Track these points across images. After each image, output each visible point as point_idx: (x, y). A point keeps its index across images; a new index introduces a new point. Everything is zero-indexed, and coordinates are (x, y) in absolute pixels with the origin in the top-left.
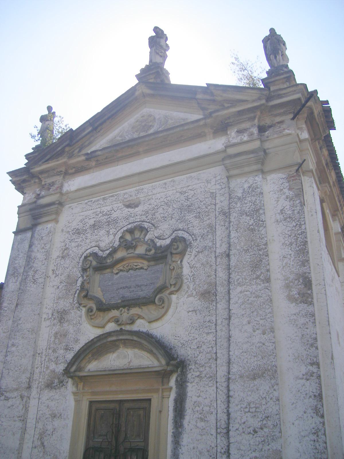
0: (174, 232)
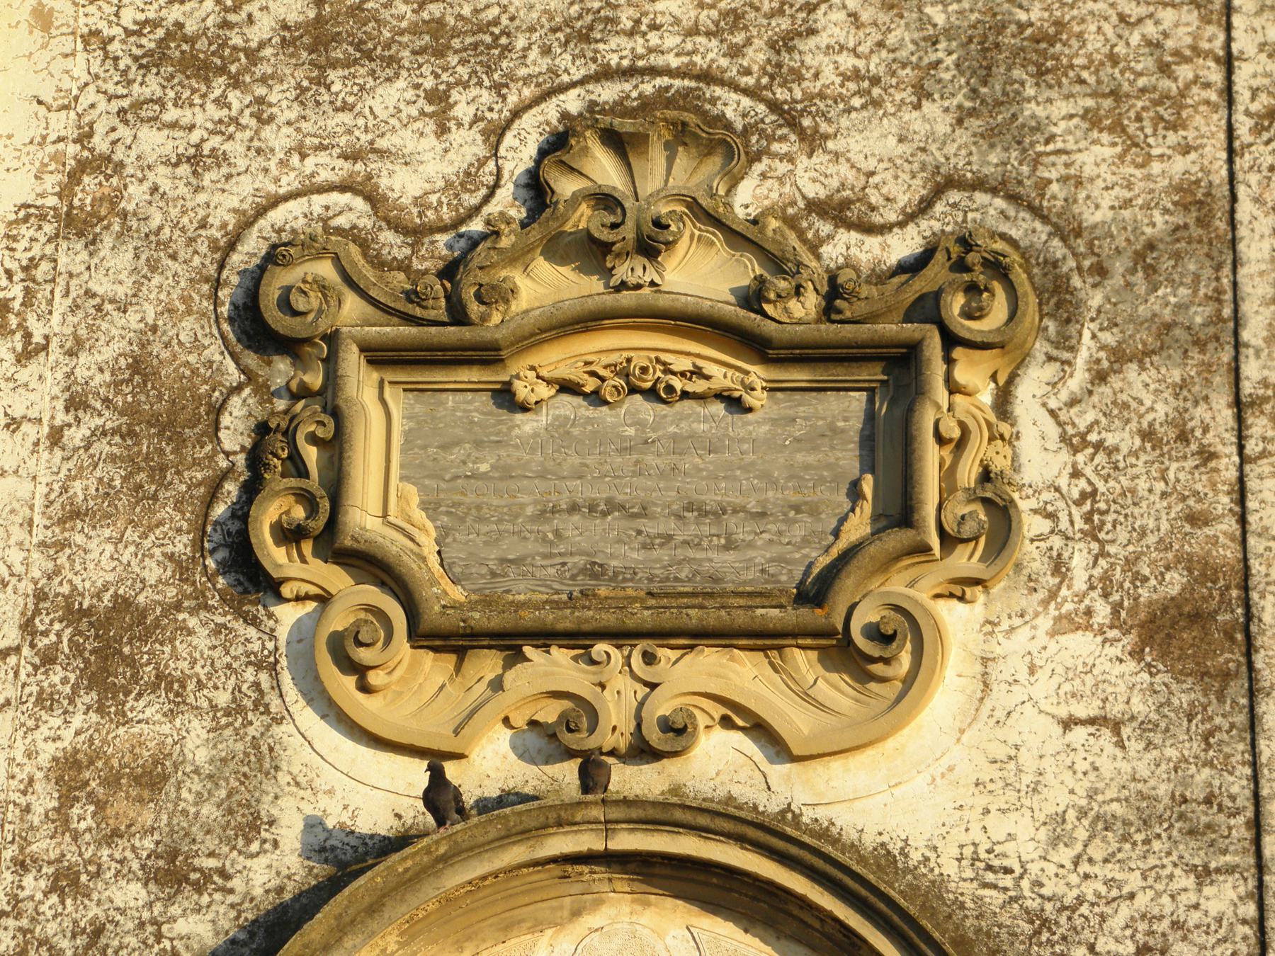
0: (938, 191)
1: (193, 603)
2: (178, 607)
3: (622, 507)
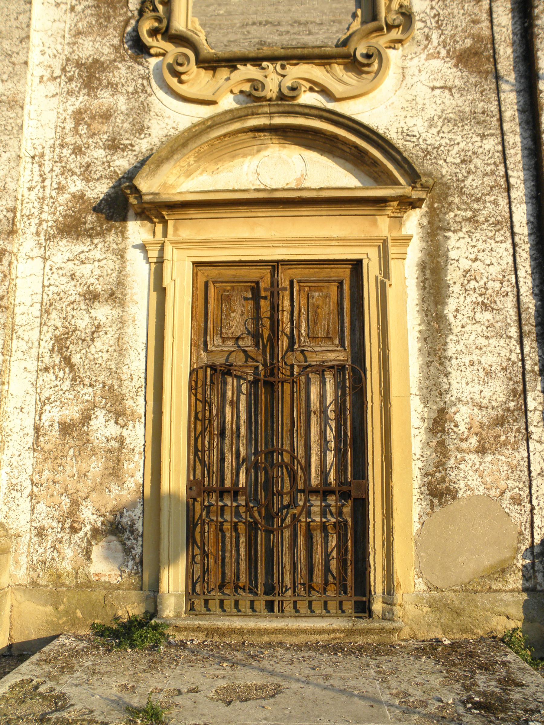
1: (120, 59)
2: (115, 61)
3: (271, 23)
